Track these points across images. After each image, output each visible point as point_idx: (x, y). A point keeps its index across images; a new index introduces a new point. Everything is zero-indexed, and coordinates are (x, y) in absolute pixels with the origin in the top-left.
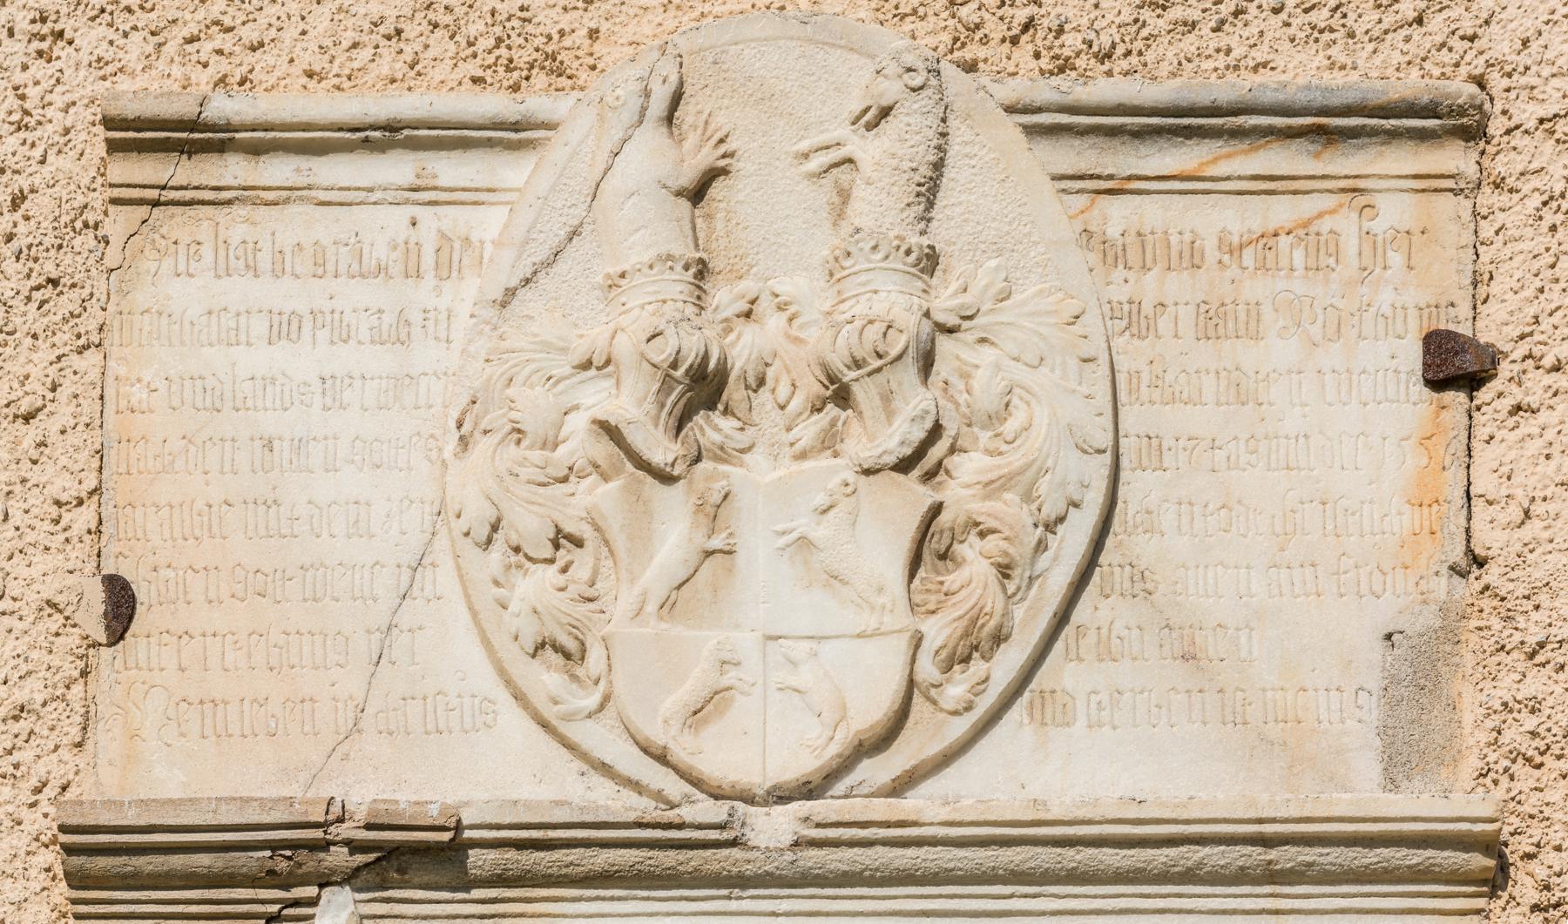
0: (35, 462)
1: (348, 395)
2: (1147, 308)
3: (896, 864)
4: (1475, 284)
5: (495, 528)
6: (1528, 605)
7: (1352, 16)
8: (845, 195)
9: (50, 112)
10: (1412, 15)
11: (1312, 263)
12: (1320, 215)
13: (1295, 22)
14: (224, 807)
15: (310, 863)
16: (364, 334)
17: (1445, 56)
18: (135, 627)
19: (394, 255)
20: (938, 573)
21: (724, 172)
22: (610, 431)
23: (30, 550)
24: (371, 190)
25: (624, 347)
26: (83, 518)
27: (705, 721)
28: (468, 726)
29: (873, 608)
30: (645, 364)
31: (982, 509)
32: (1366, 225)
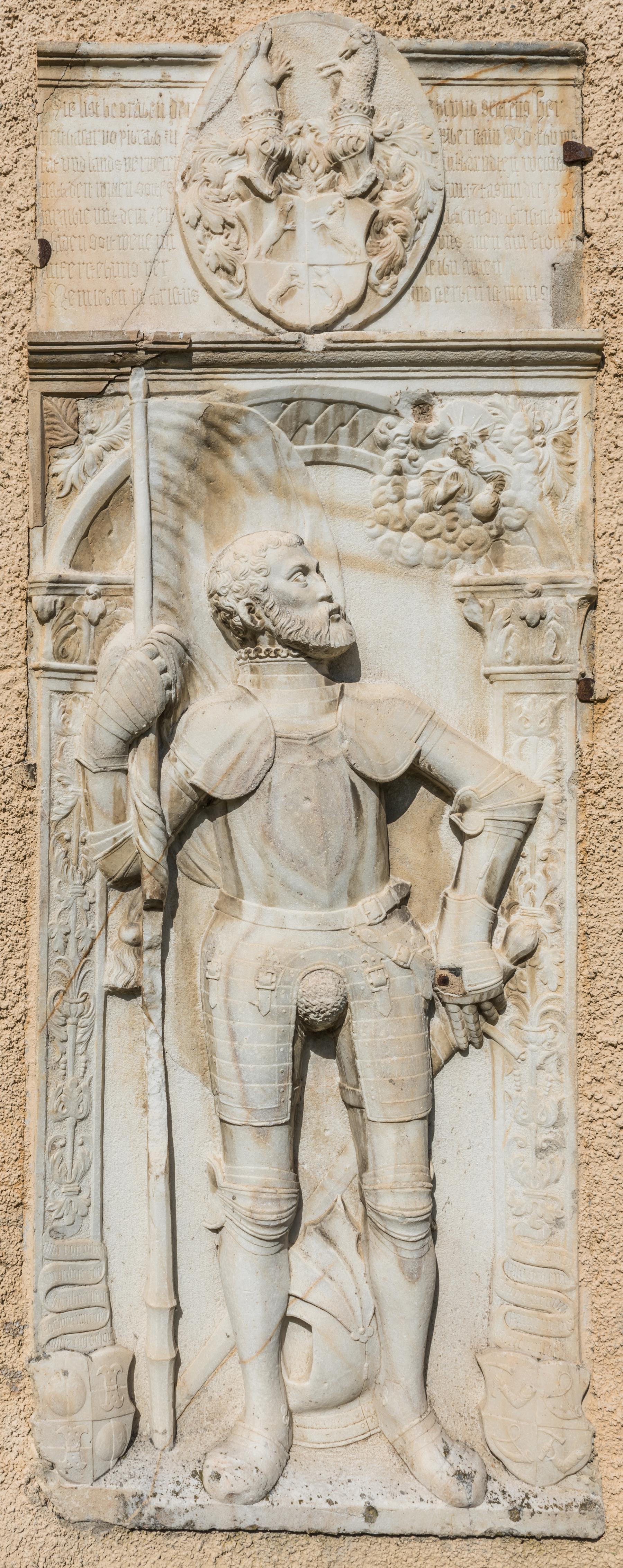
0: (9, 192)
1: (135, 165)
2: (455, 132)
3: (364, 358)
4: (583, 123)
5: (199, 220)
6: (609, 253)
7: (532, 15)
8: (337, 86)
9: (13, 49)
10: (556, 15)
11: (518, 114)
12: (522, 95)
13: (510, 17)
14: (96, 335)
15: (129, 357)
16: (142, 141)
17: (569, 31)
18: (51, 261)
19: (153, 108)
20: (377, 239)
21: (289, 76)
22: (246, 181)
23: (8, 229)
24: (143, 82)
25: (251, 147)
26: (29, 216)
27: (285, 299)
28: (187, 301)
29: (352, 253)
30: (261, 154)
31: (395, 213)
32: (540, 99)
